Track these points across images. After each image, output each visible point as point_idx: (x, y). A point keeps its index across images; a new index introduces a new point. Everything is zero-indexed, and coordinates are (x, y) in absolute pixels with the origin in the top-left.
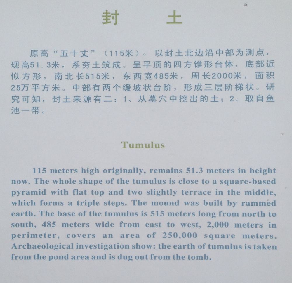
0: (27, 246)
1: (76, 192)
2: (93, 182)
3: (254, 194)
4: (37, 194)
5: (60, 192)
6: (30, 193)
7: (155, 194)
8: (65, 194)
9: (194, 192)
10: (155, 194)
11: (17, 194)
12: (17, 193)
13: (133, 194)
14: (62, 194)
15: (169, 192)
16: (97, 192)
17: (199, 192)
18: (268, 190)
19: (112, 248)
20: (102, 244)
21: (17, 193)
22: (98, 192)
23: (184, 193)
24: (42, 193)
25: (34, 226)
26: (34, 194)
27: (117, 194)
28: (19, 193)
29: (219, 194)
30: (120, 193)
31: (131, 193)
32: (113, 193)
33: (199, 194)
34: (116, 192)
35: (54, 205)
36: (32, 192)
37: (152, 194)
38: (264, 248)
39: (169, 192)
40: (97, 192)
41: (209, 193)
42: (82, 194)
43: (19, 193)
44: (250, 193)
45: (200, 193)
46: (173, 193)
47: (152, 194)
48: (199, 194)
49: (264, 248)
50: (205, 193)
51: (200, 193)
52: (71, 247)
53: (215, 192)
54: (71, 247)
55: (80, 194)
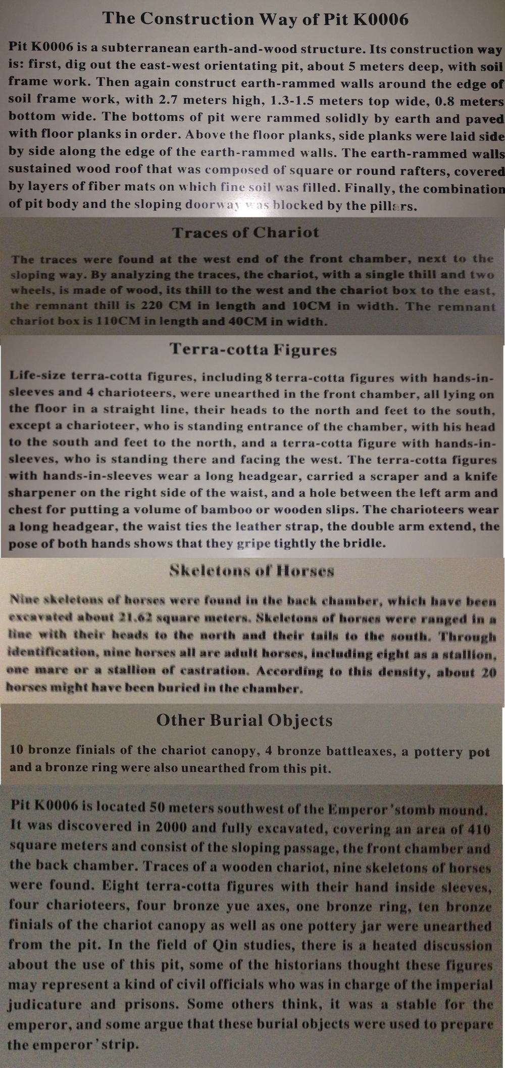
0: (366, 395)
1: (46, 134)
2: (397, 478)
3: (465, 139)
4: (437, 157)
5: (24, 134)
6: (159, 49)
7: (76, 67)
8: (222, 51)
9: (144, 48)
10: (76, 67)
11: (250, 753)
12: (199, 926)
13: (364, 495)
14: (417, 381)
15: (304, 544)
16: (377, 101)
17: (212, 348)
18: (373, 540)
19: (249, 69)
20: (230, 14)
21: (199, 926)
22: (236, 23)
23: (279, 378)
24: (95, 1025)
25: (261, 102)
26: (189, 103)
27: (247, 52)
28: (44, 188)
29: (381, 174)
30: (84, 888)
31: (475, 275)
32: (159, 49)
33: (51, 102)
34: (448, 119)
35: (415, 529)
36: (295, 117)
37: (334, 512)
38: (359, 22)
39: (304, 544)
40: (377, 101)
41: (368, 908)
42: (142, 190)
43: (44, 188)
44: (106, 866)
45: (213, 276)
46: (362, 120)
47: (334, 512)
48: (51, 102)
49: (359, 22)
50: (208, 234)
51: (213, 276)
52: (258, 722)
53: (330, 1005)
54: (258, 722)
55: (92, 137)
